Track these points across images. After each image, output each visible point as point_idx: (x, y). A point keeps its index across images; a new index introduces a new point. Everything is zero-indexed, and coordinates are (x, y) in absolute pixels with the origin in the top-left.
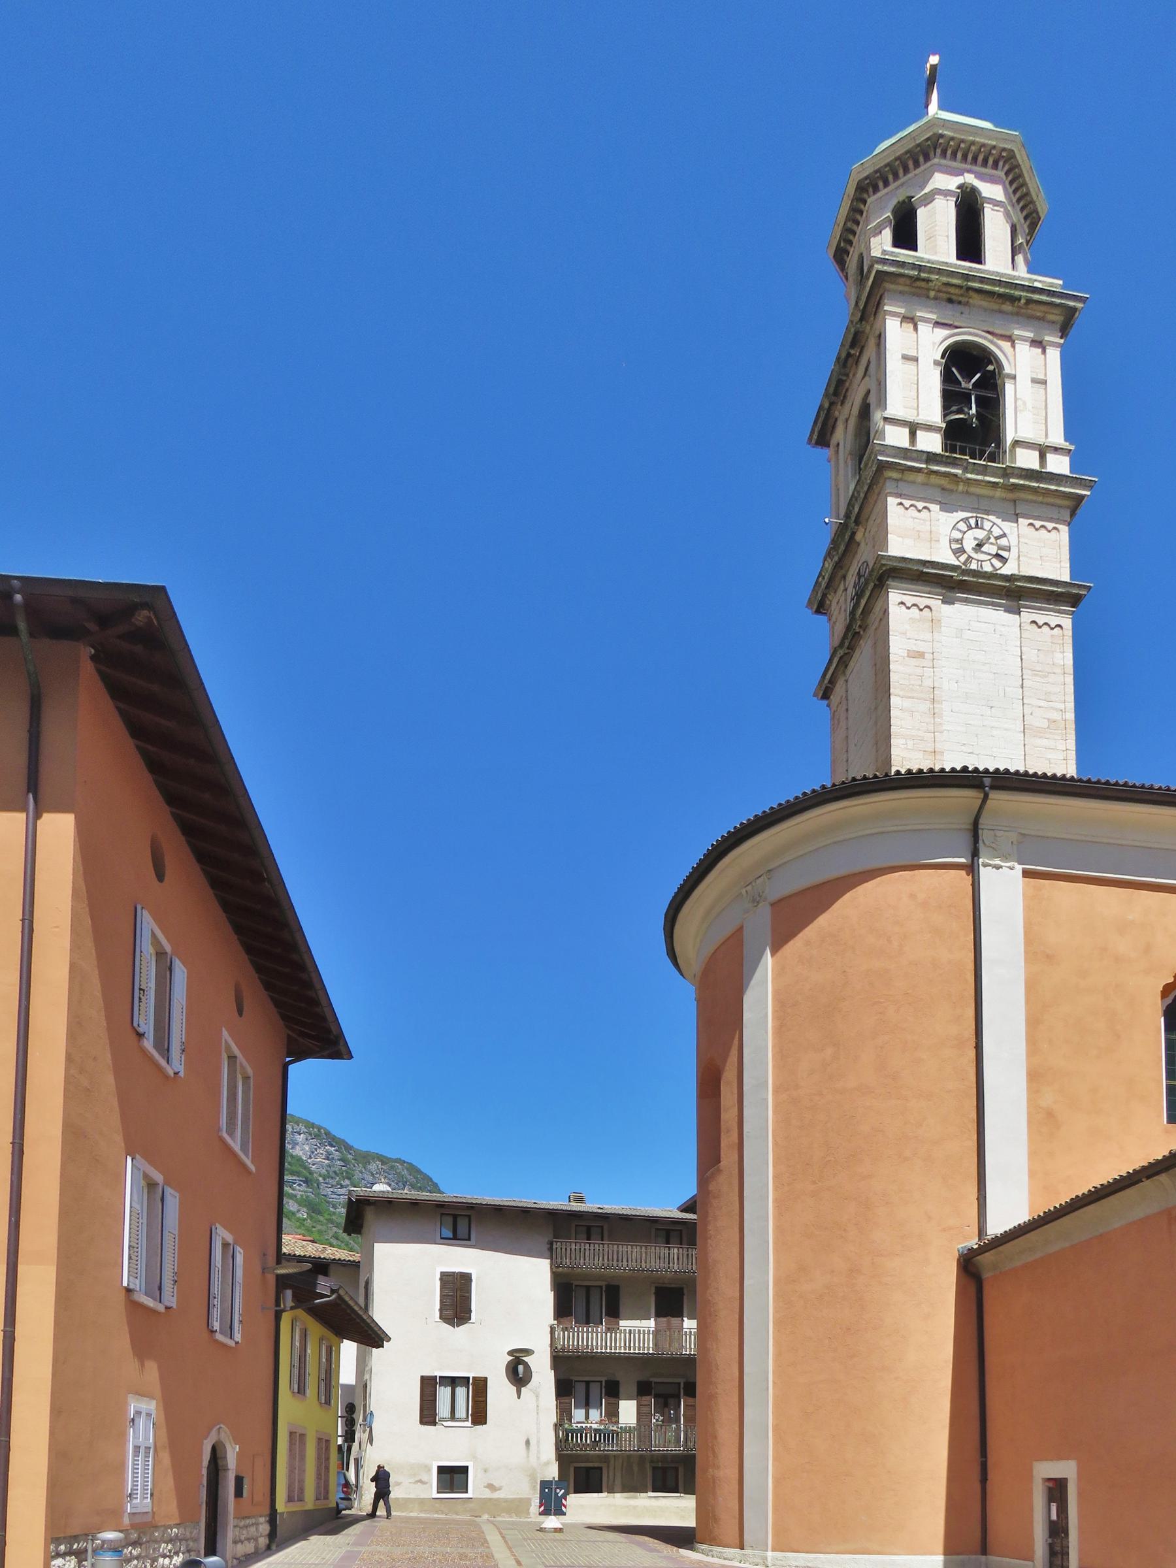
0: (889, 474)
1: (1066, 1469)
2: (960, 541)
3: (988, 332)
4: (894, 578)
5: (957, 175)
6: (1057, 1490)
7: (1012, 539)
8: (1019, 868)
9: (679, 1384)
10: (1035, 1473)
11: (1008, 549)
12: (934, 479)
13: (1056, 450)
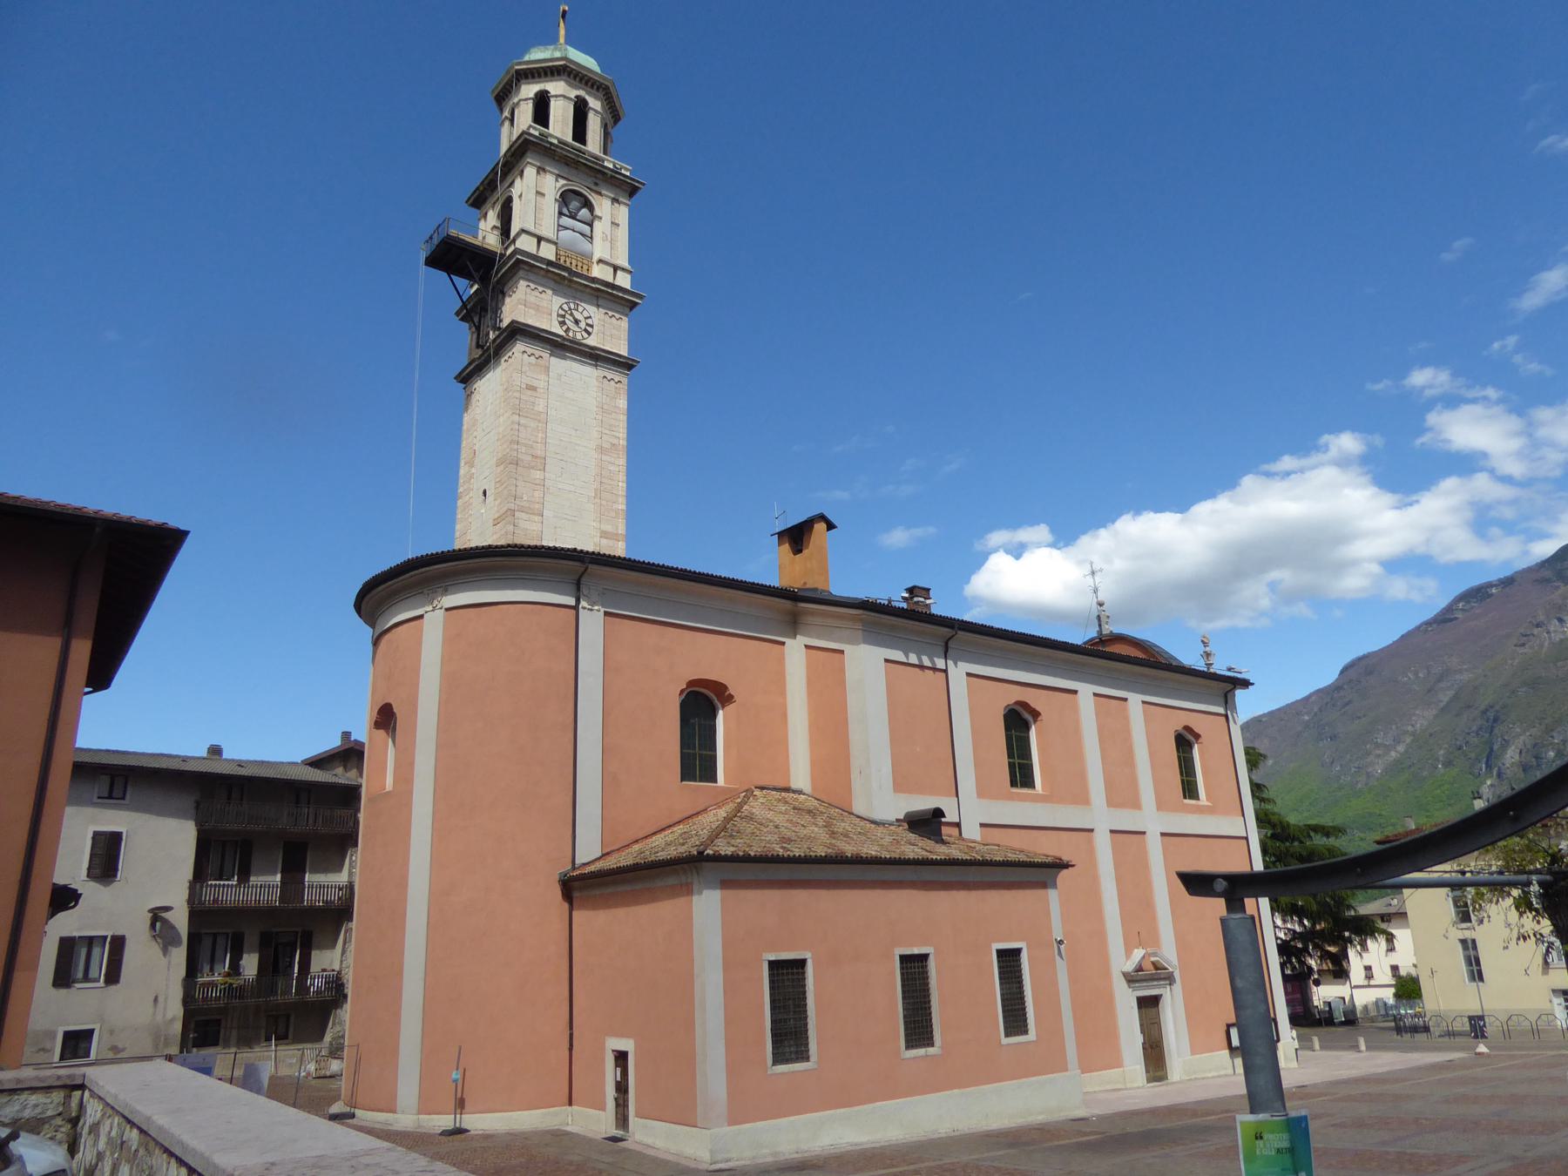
0: (522, 266)
1: (626, 1045)
2: (564, 316)
3: (588, 188)
4: (521, 334)
5: (576, 89)
6: (621, 1057)
7: (595, 321)
8: (602, 610)
9: (297, 933)
10: (607, 1045)
11: (592, 326)
12: (550, 275)
13: (623, 269)
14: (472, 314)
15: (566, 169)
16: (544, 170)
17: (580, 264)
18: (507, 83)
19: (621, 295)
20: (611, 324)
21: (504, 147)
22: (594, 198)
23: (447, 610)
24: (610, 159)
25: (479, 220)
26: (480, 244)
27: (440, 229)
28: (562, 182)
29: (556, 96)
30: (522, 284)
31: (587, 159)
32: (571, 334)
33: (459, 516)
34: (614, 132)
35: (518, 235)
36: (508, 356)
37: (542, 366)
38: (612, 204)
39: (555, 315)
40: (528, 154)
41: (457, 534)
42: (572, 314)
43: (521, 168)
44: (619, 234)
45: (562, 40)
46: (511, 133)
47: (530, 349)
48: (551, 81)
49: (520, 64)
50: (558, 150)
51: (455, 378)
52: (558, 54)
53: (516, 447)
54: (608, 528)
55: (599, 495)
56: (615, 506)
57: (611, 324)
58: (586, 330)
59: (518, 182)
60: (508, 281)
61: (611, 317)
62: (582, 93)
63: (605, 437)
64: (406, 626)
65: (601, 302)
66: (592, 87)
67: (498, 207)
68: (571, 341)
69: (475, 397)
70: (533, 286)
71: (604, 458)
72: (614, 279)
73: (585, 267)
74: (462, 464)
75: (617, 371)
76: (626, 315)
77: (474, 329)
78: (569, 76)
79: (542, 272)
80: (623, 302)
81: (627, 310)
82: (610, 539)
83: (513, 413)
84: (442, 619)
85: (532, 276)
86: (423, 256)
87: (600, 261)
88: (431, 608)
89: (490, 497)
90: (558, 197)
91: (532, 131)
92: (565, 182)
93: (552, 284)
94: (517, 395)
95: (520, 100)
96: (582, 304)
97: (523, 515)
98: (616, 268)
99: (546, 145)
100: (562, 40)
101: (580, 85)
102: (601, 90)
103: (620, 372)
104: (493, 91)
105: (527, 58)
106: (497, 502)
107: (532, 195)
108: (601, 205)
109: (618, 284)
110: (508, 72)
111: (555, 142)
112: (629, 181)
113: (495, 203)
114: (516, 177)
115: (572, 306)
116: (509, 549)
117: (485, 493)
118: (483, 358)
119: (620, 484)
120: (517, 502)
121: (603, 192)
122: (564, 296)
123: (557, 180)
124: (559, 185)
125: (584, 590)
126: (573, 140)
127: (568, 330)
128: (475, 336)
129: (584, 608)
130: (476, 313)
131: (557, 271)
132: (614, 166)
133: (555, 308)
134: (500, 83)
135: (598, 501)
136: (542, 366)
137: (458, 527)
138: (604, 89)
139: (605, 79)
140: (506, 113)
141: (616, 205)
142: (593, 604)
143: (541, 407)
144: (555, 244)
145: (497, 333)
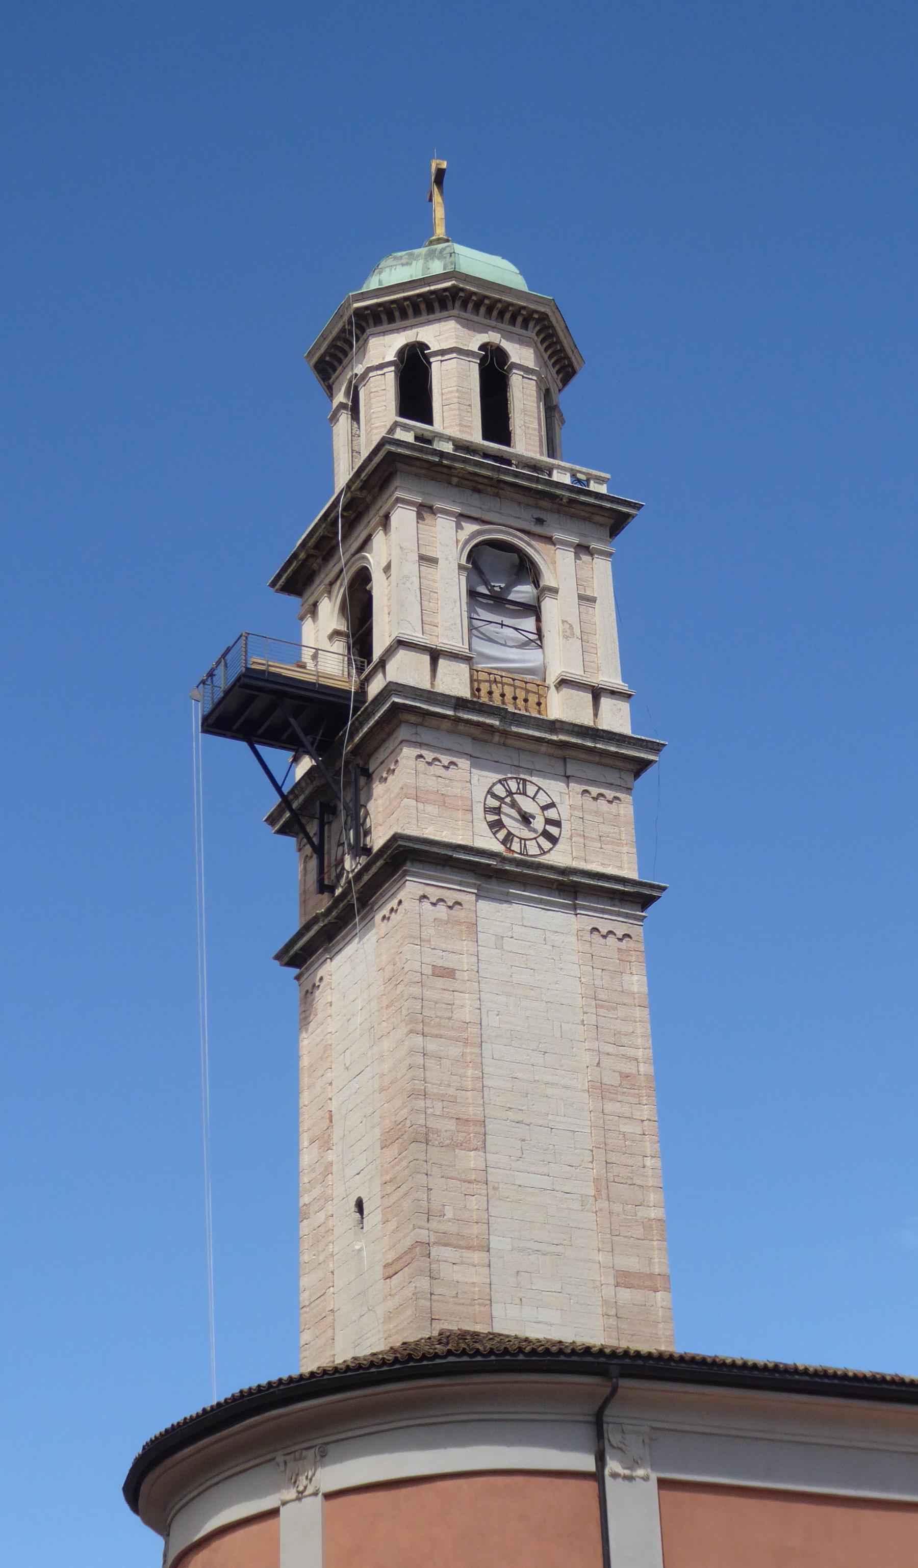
2: (497, 811)
7: (563, 812)
11: (557, 824)
12: (461, 727)
14: (304, 821)
15: (475, 499)
16: (431, 509)
17: (521, 695)
18: (338, 338)
19: (613, 749)
20: (597, 813)
21: (343, 475)
22: (537, 552)
23: (328, 1496)
24: (563, 464)
25: (302, 618)
26: (312, 679)
27: (228, 657)
28: (470, 528)
29: (443, 352)
30: (408, 753)
31: (516, 475)
32: (516, 846)
33: (305, 1257)
34: (564, 399)
35: (390, 652)
36: (389, 907)
37: (461, 923)
38: (577, 557)
39: (479, 810)
40: (397, 482)
41: (304, 1297)
42: (514, 805)
43: (382, 512)
44: (597, 619)
45: (440, 231)
46: (354, 436)
47: (433, 889)
48: (429, 322)
49: (359, 298)
50: (457, 465)
51: (278, 957)
52: (437, 267)
53: (421, 1103)
54: (631, 1263)
55: (604, 1193)
56: (642, 1212)
57: (597, 813)
58: (546, 834)
59: (379, 538)
60: (376, 749)
61: (595, 799)
62: (493, 337)
63: (606, 1062)
64: (241, 1533)
65: (571, 769)
66: (513, 321)
67: (340, 591)
68: (519, 863)
69: (322, 998)
70: (429, 755)
71: (610, 1107)
72: (596, 715)
73: (533, 699)
74: (304, 1141)
75: (619, 914)
76: (629, 790)
77: (308, 849)
78: (464, 306)
79: (446, 724)
80: (619, 764)
81: (629, 778)
82: (639, 1287)
83: (411, 1031)
84: (318, 1517)
85: (426, 736)
86: (197, 713)
87: (563, 683)
88: (292, 1494)
89: (373, 1216)
90: (463, 561)
91: (400, 435)
92: (475, 527)
93: (468, 746)
94: (416, 990)
95: (370, 369)
96: (534, 779)
97: (447, 1253)
98: (597, 693)
99: (430, 458)
100: (440, 231)
101: (487, 322)
102: (531, 324)
103: (627, 916)
104: (311, 354)
105: (373, 283)
106: (391, 1225)
107: (411, 566)
108: (554, 563)
109: (605, 727)
110: (339, 315)
111: (448, 448)
112: (608, 505)
113: (332, 584)
114: (374, 529)
115: (513, 786)
116: (451, 1359)
117: (359, 1205)
118: (334, 914)
119: (649, 1162)
120: (434, 1225)
121: (557, 535)
122: (494, 765)
123: (459, 527)
124: (464, 535)
125: (613, 1436)
126: (485, 437)
127: (509, 838)
128: (313, 863)
129: (615, 1475)
130: (312, 817)
131: (475, 718)
132: (573, 476)
133: (479, 794)
134: (324, 337)
135: (604, 1204)
136: (461, 923)
137: (305, 1281)
138: (538, 321)
139: (538, 300)
140: (340, 397)
141: (586, 558)
142: (635, 1463)
143: (467, 1013)
144: (467, 659)
145: (363, 860)
